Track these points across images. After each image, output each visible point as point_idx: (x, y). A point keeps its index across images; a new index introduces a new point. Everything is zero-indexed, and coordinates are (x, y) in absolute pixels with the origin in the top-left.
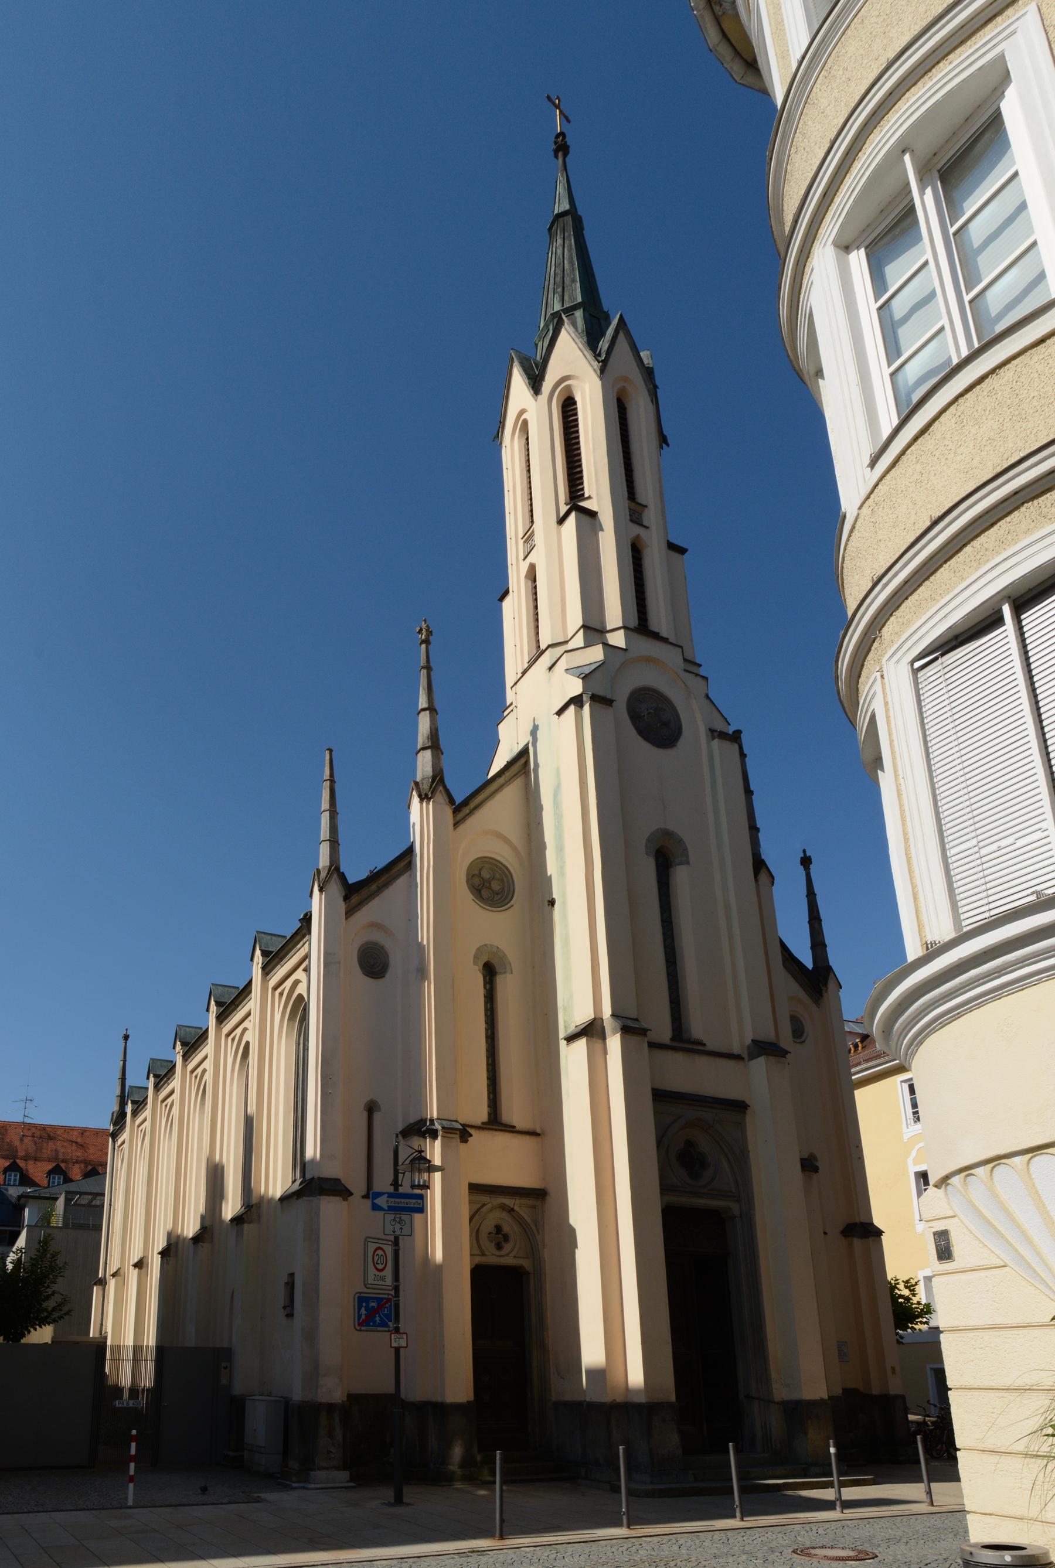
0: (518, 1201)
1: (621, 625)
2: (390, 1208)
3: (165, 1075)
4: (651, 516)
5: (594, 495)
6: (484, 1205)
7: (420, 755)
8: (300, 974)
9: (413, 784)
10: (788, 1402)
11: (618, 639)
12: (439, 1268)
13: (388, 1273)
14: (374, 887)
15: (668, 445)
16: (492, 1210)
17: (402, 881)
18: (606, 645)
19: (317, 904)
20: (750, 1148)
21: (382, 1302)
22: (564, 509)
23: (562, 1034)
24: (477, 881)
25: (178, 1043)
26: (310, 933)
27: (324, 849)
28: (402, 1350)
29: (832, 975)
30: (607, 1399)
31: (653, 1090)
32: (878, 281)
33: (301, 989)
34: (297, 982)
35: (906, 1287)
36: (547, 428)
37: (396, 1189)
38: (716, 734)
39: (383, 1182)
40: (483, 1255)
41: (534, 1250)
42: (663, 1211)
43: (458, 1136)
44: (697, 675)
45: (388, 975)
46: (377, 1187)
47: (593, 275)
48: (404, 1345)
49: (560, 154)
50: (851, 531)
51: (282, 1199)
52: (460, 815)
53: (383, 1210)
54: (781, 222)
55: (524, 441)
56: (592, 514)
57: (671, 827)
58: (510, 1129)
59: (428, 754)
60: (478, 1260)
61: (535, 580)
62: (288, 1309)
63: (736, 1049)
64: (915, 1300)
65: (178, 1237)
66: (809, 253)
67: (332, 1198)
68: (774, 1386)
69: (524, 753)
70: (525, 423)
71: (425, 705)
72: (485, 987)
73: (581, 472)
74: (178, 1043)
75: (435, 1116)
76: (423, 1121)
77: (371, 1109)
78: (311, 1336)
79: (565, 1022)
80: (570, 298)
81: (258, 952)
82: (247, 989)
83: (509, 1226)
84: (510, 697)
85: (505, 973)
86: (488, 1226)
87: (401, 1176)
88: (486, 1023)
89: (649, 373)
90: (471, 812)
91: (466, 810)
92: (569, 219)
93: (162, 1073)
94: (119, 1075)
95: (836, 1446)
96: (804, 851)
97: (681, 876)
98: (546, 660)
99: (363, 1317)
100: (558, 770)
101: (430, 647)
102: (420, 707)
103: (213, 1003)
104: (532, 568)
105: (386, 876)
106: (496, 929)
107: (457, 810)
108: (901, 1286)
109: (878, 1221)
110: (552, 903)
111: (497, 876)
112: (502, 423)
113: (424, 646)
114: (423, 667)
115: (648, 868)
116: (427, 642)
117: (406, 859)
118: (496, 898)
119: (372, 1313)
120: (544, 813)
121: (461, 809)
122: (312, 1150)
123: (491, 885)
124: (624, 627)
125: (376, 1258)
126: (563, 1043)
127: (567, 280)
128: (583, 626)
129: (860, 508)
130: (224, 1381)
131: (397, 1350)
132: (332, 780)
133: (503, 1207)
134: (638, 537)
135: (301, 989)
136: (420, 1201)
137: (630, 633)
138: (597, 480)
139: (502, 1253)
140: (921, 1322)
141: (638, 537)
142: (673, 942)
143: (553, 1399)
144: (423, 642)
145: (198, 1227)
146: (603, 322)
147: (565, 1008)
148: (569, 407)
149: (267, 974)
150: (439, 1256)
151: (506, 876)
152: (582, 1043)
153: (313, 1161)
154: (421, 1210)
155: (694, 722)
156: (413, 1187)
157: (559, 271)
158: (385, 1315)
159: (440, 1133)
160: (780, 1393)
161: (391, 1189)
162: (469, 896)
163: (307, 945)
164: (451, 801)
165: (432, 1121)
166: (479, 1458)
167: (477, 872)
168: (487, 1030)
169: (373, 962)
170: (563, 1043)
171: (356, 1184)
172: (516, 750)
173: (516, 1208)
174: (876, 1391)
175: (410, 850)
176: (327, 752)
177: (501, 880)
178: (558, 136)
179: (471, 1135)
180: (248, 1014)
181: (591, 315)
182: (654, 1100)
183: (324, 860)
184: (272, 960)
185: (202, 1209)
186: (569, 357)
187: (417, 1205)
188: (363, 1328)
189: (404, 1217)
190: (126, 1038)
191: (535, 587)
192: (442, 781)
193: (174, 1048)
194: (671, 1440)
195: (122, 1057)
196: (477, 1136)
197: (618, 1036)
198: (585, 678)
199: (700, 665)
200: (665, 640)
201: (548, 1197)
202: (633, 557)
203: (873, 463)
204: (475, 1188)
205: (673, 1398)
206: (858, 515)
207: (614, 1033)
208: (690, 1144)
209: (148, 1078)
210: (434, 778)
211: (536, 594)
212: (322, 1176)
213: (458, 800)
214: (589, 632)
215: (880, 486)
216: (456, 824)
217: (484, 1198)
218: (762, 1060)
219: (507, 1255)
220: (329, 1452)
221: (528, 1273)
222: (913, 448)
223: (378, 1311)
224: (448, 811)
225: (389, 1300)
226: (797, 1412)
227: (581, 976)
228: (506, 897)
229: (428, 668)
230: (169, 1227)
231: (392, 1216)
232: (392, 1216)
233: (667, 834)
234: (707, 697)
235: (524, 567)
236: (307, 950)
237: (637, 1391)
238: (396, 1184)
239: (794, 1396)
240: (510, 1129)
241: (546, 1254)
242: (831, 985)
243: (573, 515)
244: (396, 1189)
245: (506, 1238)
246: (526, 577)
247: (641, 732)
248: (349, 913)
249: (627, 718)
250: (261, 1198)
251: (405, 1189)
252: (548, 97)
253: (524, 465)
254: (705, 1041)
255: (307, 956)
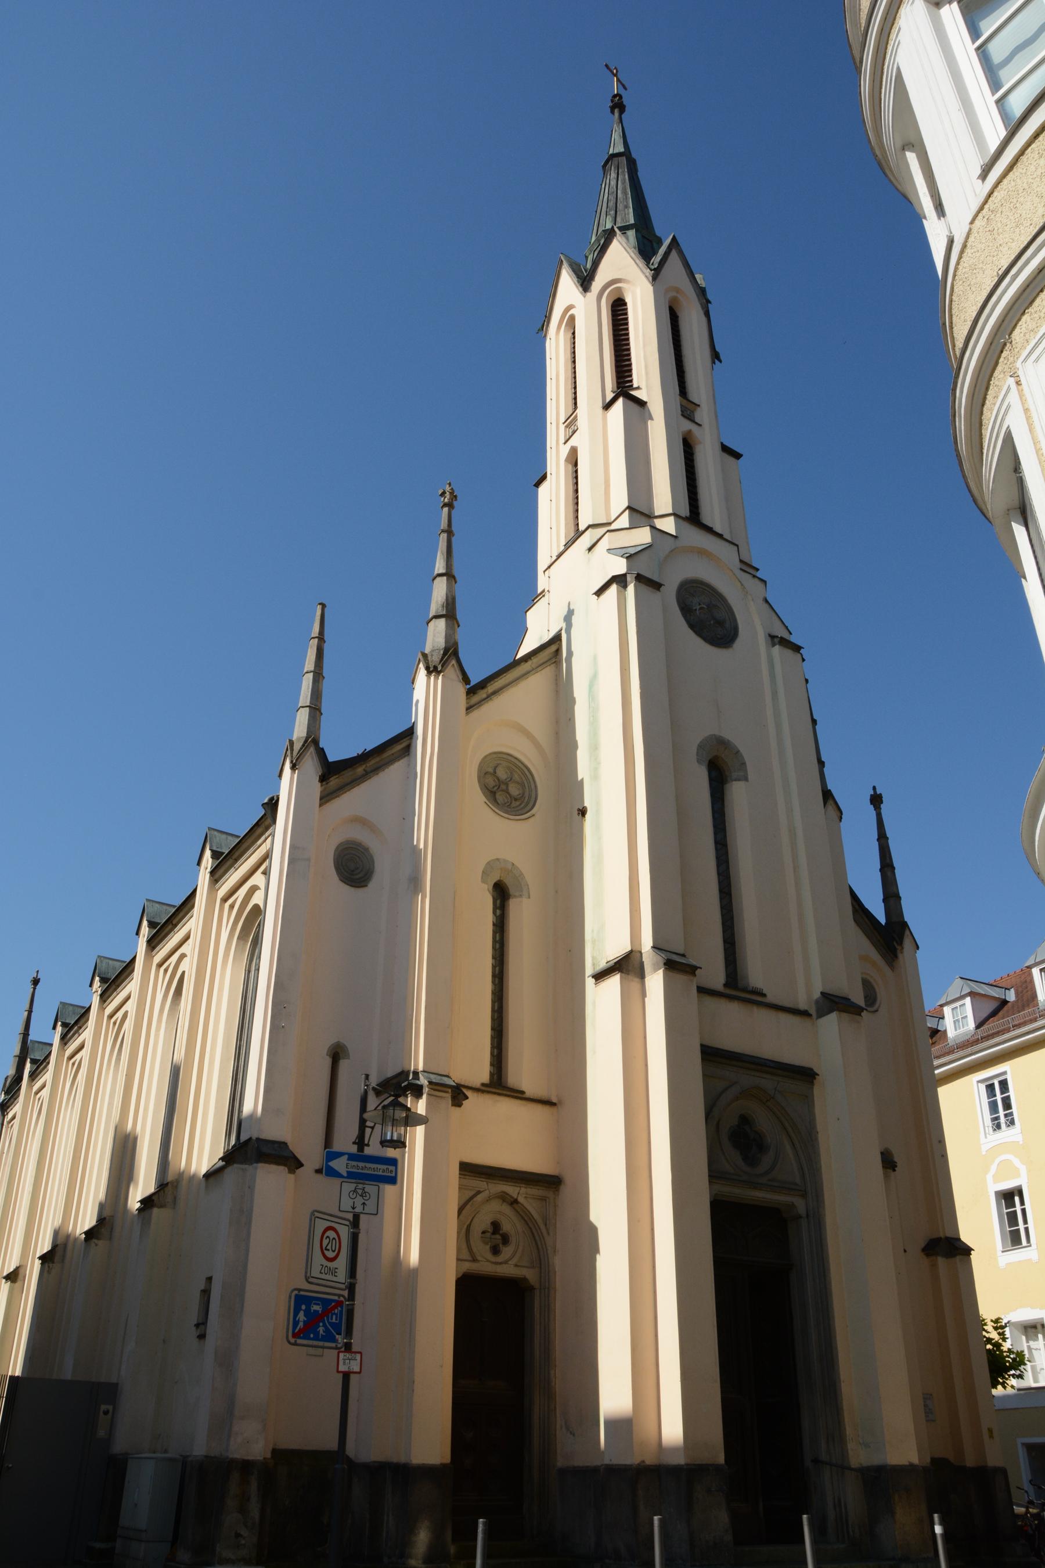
0: (523, 1190)
1: (671, 511)
2: (351, 1175)
3: (76, 1023)
4: (703, 415)
5: (643, 386)
6: (479, 1192)
7: (431, 624)
8: (258, 879)
9: (420, 656)
10: (869, 1469)
11: (668, 525)
12: (414, 1273)
13: (341, 1264)
14: (360, 770)
15: (720, 361)
16: (488, 1200)
17: (396, 769)
18: (653, 528)
19: (287, 787)
20: (819, 1127)
21: (329, 1306)
22: (610, 396)
23: (589, 971)
24: (490, 781)
25: (97, 979)
26: (274, 821)
27: (302, 719)
28: (353, 1378)
29: (907, 932)
30: (634, 1460)
31: (702, 1046)
32: (974, 33)
33: (257, 899)
34: (254, 889)
35: (996, 1328)
36: (592, 344)
37: (361, 1149)
38: (774, 640)
39: (345, 1140)
40: (474, 1260)
41: (541, 1260)
42: (712, 1203)
43: (448, 1096)
44: (754, 576)
45: (372, 884)
46: (337, 1147)
47: (646, 207)
48: (357, 1369)
49: (616, 111)
50: (962, 252)
51: (208, 1176)
52: (475, 699)
53: (342, 1177)
54: (856, 22)
55: (570, 335)
56: (642, 404)
57: (727, 735)
58: (518, 1094)
59: (441, 623)
60: (467, 1266)
61: (576, 465)
62: (202, 1327)
63: (802, 1006)
64: (1006, 1346)
65: (68, 1236)
66: (895, 19)
67: (273, 1167)
68: (850, 1446)
69: (557, 639)
70: (572, 318)
71: (442, 571)
72: (494, 913)
73: (630, 365)
74: (97, 979)
75: (421, 1068)
76: (404, 1074)
77: (337, 1055)
78: (227, 1360)
79: (593, 958)
80: (622, 220)
81: (208, 853)
82: (188, 902)
83: (510, 1224)
84: (542, 584)
85: (521, 896)
86: (483, 1222)
87: (368, 1131)
88: (494, 958)
89: (702, 292)
90: (489, 697)
91: (482, 694)
92: (624, 160)
93: (72, 1022)
94: (20, 1028)
95: (942, 1523)
96: (874, 788)
97: (737, 793)
98: (586, 540)
99: (301, 1325)
100: (595, 658)
101: (453, 512)
102: (436, 572)
103: (145, 923)
104: (574, 451)
105: (378, 759)
106: (511, 841)
107: (471, 692)
108: (989, 1327)
109: (966, 1237)
110: (583, 812)
111: (516, 777)
112: (548, 318)
113: (446, 509)
114: (443, 531)
115: (700, 779)
116: (450, 505)
117: (404, 741)
118: (515, 804)
119: (313, 1321)
120: (577, 708)
121: (478, 691)
122: (252, 1103)
123: (508, 788)
124: (674, 514)
125: (325, 1242)
126: (590, 982)
127: (620, 206)
128: (629, 507)
129: (972, 223)
130: (101, 1433)
131: (346, 1376)
132: (321, 638)
133: (503, 1197)
134: (690, 431)
135: (257, 899)
136: (392, 1168)
137: (680, 521)
138: (647, 373)
139: (501, 1258)
140: (1013, 1376)
141: (690, 431)
142: (728, 868)
143: (560, 1463)
144: (445, 505)
145: (94, 1223)
146: (655, 244)
147: (594, 942)
148: (618, 309)
149: (217, 881)
150: (414, 1257)
151: (527, 779)
152: (615, 981)
153: (252, 1116)
154: (393, 1180)
155: (752, 624)
156: (384, 1143)
157: (612, 198)
158: (331, 1324)
159: (426, 1090)
160: (859, 1456)
161: (354, 1149)
162: (479, 797)
163: (270, 838)
164: (466, 679)
165: (416, 1074)
166: (452, 1550)
167: (491, 770)
168: (494, 967)
169: (354, 867)
170: (590, 982)
171: (309, 1149)
172: (546, 638)
173: (521, 1199)
174: (970, 1461)
175: (410, 732)
176: (319, 607)
177: (523, 785)
178: (615, 96)
179: (467, 1098)
180: (187, 938)
181: (643, 237)
182: (703, 1059)
183: (300, 730)
184: (224, 862)
185: (101, 1195)
186: (620, 262)
187: (389, 1173)
188: (299, 1341)
189: (368, 1188)
190: (36, 982)
191: (576, 471)
192: (456, 654)
193: (91, 985)
194: (717, 1519)
195: (27, 1007)
196: (473, 1101)
197: (661, 972)
198: (630, 558)
199: (758, 570)
200: (720, 536)
201: (562, 1187)
202: (685, 451)
203: (984, 175)
204: (468, 1169)
205: (721, 1459)
206: (970, 230)
207: (656, 970)
208: (745, 1120)
209: (54, 1028)
210: (446, 650)
211: (577, 477)
212: (263, 1136)
213: (474, 680)
214: (635, 514)
215: (995, 194)
216: (469, 709)
217: (480, 1184)
218: (834, 1016)
219: (506, 1262)
220: (238, 1535)
221: (532, 1289)
222: (1033, 146)
223: (322, 1318)
224: (461, 690)
225: (339, 1304)
226: (880, 1480)
227: (616, 898)
228: (527, 804)
229: (449, 532)
230: (57, 1223)
231: (353, 1186)
232: (353, 1186)
233: (722, 743)
234: (766, 601)
235: (565, 450)
236: (268, 847)
237: (674, 1450)
238: (361, 1142)
239: (876, 1460)
240: (518, 1094)
241: (557, 1262)
242: (907, 943)
243: (620, 400)
244: (361, 1149)
245: (506, 1239)
246: (567, 460)
247: (692, 626)
248: (326, 798)
249: (677, 609)
250: (181, 1175)
251: (373, 1149)
252: (606, 66)
253: (569, 356)
254: (765, 992)
255: (267, 856)
